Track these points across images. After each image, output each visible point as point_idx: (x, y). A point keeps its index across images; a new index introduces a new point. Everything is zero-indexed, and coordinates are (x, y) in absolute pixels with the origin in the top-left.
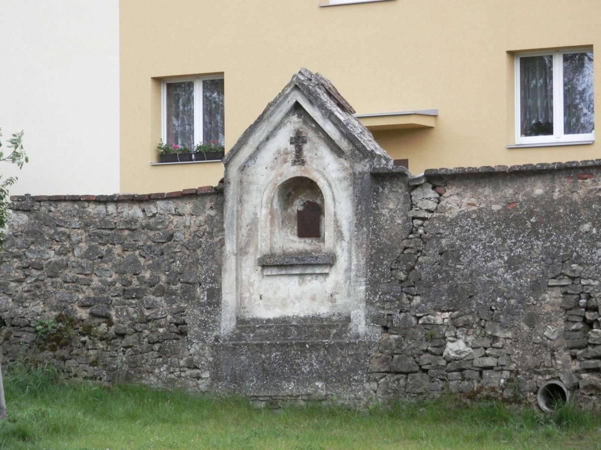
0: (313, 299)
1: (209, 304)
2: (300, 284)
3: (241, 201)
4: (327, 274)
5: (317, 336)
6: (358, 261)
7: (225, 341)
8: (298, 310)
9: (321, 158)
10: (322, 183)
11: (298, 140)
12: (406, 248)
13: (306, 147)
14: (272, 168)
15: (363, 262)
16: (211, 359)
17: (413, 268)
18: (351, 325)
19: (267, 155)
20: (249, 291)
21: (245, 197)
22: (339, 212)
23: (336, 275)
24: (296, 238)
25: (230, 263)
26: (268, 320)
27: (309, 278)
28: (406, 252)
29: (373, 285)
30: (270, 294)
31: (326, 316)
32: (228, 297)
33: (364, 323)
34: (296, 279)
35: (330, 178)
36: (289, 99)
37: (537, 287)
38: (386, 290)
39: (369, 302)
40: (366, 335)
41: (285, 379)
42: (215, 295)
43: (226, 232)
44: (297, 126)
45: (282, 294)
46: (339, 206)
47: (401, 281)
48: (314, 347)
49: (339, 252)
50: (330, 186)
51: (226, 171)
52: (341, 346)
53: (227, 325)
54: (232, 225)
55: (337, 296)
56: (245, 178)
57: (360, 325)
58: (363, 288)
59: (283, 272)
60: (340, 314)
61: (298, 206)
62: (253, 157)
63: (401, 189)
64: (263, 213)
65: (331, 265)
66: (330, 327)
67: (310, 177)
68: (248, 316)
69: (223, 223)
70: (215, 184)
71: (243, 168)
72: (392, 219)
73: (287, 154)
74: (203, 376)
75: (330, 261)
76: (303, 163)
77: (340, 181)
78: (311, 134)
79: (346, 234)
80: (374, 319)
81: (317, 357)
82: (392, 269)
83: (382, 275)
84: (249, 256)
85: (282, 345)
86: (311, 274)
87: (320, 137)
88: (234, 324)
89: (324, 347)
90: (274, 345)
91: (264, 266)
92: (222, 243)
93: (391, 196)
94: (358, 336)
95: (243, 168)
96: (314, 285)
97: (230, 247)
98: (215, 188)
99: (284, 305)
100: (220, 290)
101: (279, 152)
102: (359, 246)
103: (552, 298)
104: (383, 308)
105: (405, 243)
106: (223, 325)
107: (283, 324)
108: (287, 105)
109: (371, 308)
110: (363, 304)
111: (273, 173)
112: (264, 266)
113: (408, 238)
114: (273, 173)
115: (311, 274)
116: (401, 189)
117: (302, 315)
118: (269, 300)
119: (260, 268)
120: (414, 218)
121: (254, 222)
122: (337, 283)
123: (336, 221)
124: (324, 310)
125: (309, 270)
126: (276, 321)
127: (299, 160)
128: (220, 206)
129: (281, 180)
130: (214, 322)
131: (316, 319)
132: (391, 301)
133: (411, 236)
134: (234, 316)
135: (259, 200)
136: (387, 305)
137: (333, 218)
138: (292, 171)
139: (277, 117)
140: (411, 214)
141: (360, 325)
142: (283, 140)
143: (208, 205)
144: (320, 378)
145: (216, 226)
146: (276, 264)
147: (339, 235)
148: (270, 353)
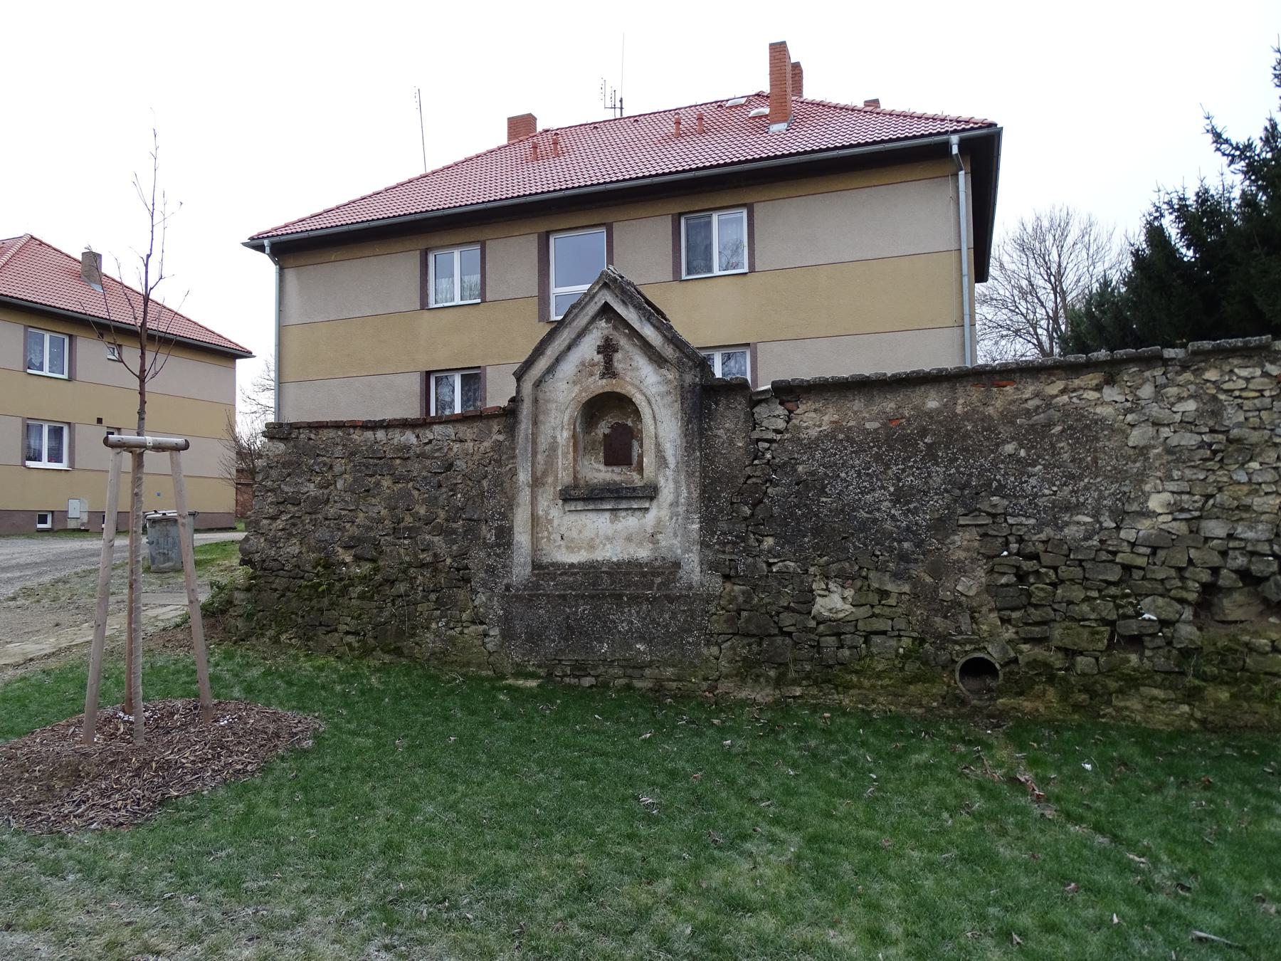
0: (629, 539)
1: (499, 545)
2: (612, 522)
3: (535, 423)
4: (647, 509)
5: (636, 585)
6: (690, 493)
7: (518, 590)
8: (610, 553)
9: (637, 369)
10: (638, 399)
11: (608, 349)
12: (749, 477)
13: (618, 356)
14: (575, 383)
15: (695, 495)
16: (501, 612)
17: (761, 501)
18: (681, 573)
19: (568, 367)
20: (547, 530)
21: (541, 417)
22: (661, 434)
23: (657, 513)
24: (602, 467)
25: (524, 496)
26: (572, 565)
27: (623, 514)
28: (749, 482)
29: (708, 523)
30: (574, 534)
31: (646, 560)
32: (522, 538)
33: (698, 569)
34: (607, 515)
35: (648, 393)
36: (596, 299)
37: (943, 525)
38: (726, 529)
39: (704, 544)
40: (702, 585)
41: (596, 639)
42: (505, 536)
43: (519, 459)
44: (606, 332)
45: (588, 534)
46: (663, 427)
47: (746, 519)
48: (634, 599)
49: (662, 482)
50: (649, 402)
51: (518, 386)
52: (671, 599)
53: (520, 570)
54: (526, 450)
55: (659, 537)
56: (541, 395)
57: (693, 569)
58: (696, 526)
59: (591, 507)
60: (664, 559)
61: (603, 429)
62: (551, 370)
63: (740, 404)
64: (564, 436)
65: (652, 499)
66: (653, 574)
67: (623, 392)
68: (545, 560)
69: (514, 449)
70: (504, 403)
71: (538, 384)
72: (731, 442)
73: (594, 365)
74: (492, 633)
75: (651, 493)
76: (614, 375)
77: (662, 396)
78: (623, 342)
79: (672, 461)
80: (710, 566)
81: (638, 613)
82: (732, 503)
83: (721, 511)
84: (547, 487)
85: (592, 597)
86: (626, 509)
87: (635, 345)
88: (529, 569)
89: (648, 599)
90: (583, 596)
91: (565, 500)
92: (514, 473)
93: (728, 413)
94: (690, 587)
95: (538, 384)
96: (630, 522)
97: (523, 477)
98: (504, 409)
99: (591, 547)
100: (511, 529)
101: (583, 364)
102: (690, 475)
103: (962, 543)
104: (724, 552)
105: (748, 471)
106: (515, 571)
107: (591, 570)
108: (593, 309)
109: (707, 552)
110: (696, 548)
111: (577, 389)
112: (565, 500)
113: (751, 464)
114: (577, 389)
115: (626, 509)
116: (740, 404)
117: (615, 559)
118: (572, 540)
119: (560, 502)
120: (758, 440)
121: (553, 447)
122: (659, 521)
123: (658, 445)
124: (643, 553)
125: (623, 506)
126: (581, 566)
127: (609, 371)
128: (511, 430)
129: (585, 397)
130: (504, 567)
131: (633, 564)
132: (734, 544)
133: (756, 462)
134: (529, 560)
135: (558, 421)
136: (728, 548)
137: (653, 441)
138: (599, 385)
139: (582, 321)
140: (755, 435)
141: (693, 569)
142: (588, 349)
143: (496, 428)
144: (642, 639)
145: (503, 455)
146: (582, 496)
147: (662, 461)
148: (577, 606)
